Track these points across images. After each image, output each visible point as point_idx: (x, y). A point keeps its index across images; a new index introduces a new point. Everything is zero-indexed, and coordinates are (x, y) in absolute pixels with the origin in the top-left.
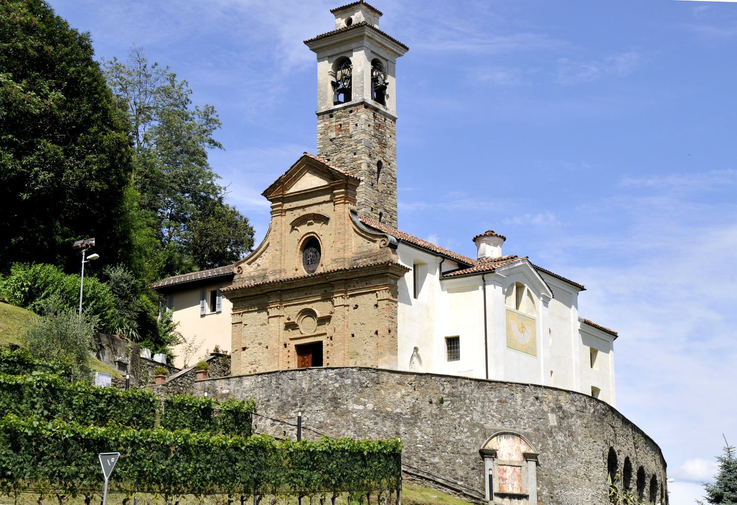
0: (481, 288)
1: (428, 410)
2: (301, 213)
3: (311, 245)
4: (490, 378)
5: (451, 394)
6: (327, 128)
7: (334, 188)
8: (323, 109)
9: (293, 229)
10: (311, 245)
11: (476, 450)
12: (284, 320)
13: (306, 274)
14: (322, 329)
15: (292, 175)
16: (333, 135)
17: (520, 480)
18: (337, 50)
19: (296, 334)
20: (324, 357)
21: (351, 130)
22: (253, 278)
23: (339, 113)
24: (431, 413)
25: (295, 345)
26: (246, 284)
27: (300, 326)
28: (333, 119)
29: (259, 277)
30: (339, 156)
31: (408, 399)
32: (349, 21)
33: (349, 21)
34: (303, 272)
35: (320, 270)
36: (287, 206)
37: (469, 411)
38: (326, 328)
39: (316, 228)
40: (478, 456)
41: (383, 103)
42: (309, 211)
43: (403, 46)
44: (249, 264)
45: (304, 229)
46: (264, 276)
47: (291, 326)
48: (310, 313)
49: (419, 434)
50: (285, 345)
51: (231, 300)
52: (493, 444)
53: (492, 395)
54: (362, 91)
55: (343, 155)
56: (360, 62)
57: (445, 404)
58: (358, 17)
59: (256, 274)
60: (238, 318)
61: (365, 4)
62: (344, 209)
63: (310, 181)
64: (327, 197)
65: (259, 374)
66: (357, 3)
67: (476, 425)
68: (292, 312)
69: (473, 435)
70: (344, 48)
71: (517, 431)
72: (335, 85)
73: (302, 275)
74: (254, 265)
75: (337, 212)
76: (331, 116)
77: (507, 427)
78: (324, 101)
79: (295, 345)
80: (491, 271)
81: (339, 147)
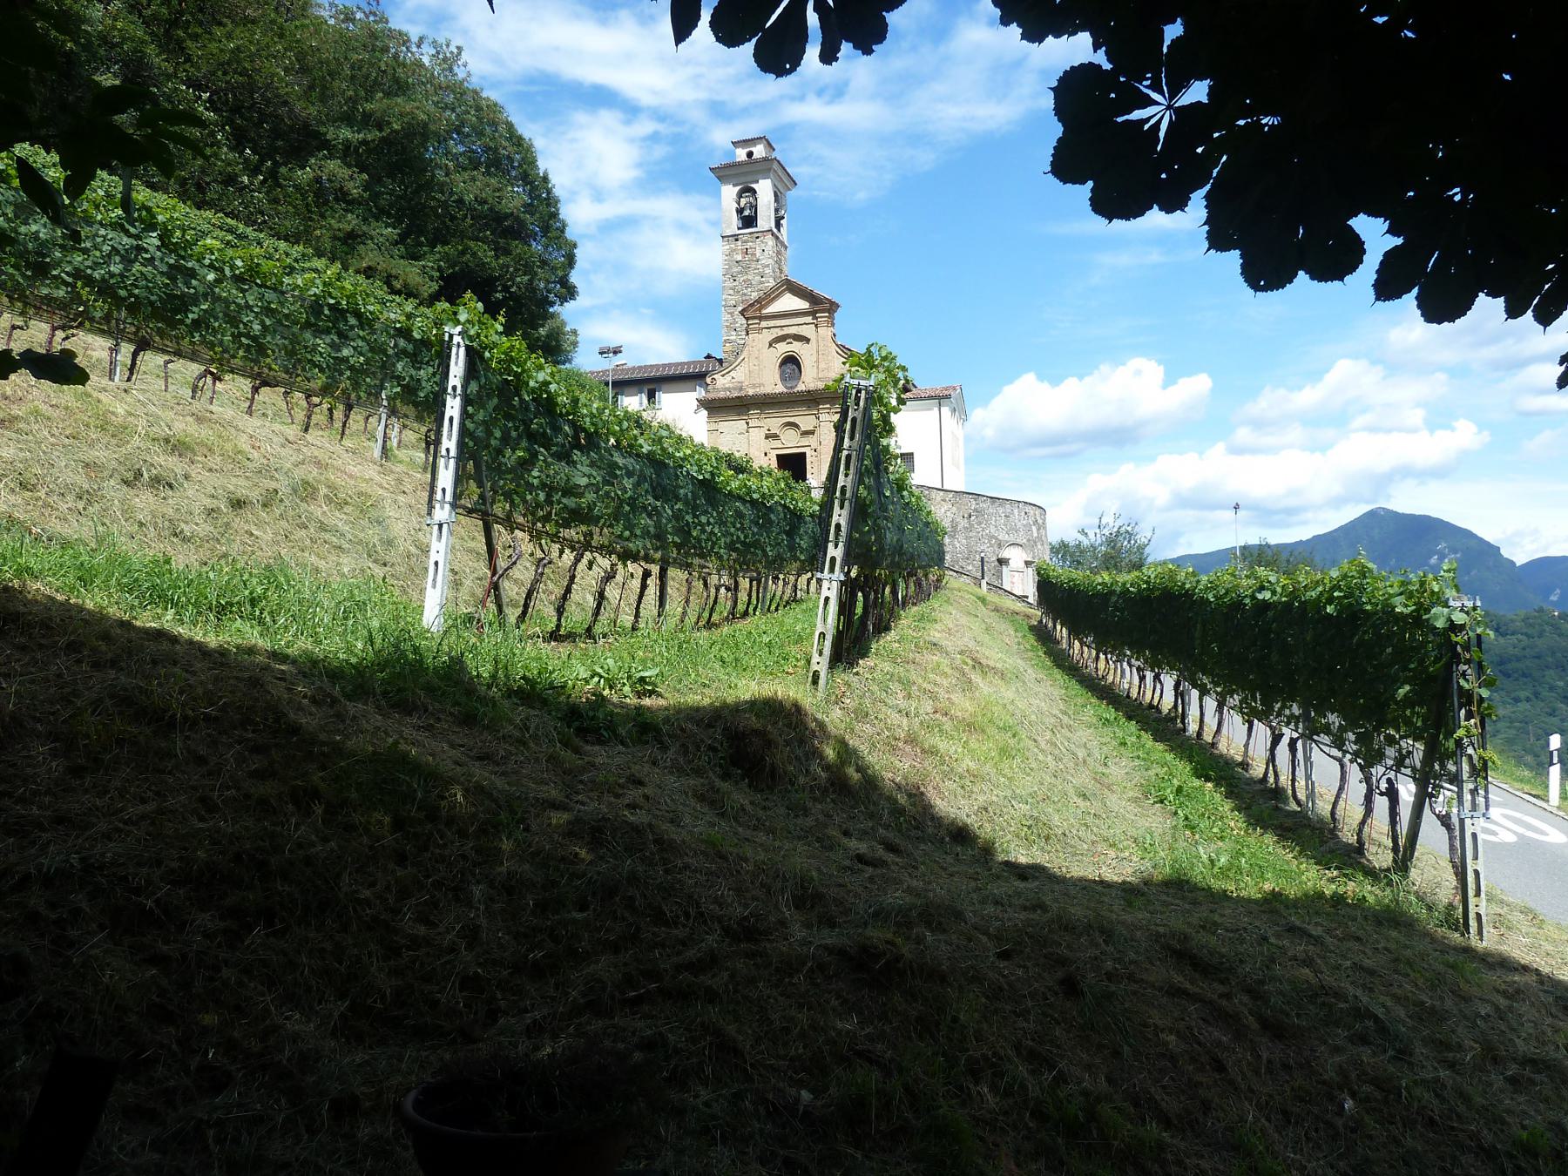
0: (936, 409)
1: (963, 523)
2: (780, 333)
3: (791, 363)
4: (945, 488)
5: (975, 510)
6: (733, 251)
7: (817, 312)
8: (729, 233)
9: (770, 345)
10: (791, 363)
11: (994, 558)
12: (764, 432)
13: (785, 390)
14: (805, 441)
15: (770, 297)
16: (739, 258)
17: (1023, 584)
18: (743, 179)
19: (777, 444)
20: (808, 467)
21: (758, 255)
22: (729, 389)
23: (745, 238)
24: (964, 527)
25: (778, 456)
26: (722, 395)
27: (782, 437)
28: (739, 243)
29: (735, 389)
30: (745, 277)
31: (948, 514)
32: (750, 154)
33: (750, 154)
34: (780, 389)
35: (801, 387)
36: (764, 324)
37: (988, 525)
38: (812, 441)
39: (796, 347)
40: (996, 563)
41: (779, 231)
42: (786, 331)
43: (794, 182)
44: (723, 376)
45: (783, 348)
46: (741, 389)
47: (771, 436)
48: (795, 425)
49: (958, 545)
50: (766, 454)
51: (706, 409)
52: (1005, 554)
53: (1001, 510)
54: (765, 220)
55: (750, 277)
56: (764, 188)
57: (973, 518)
58: (759, 151)
59: (731, 385)
60: (714, 426)
61: (767, 140)
62: (825, 332)
63: (789, 302)
64: (809, 319)
65: (343, 431)
66: (761, 138)
67: (993, 537)
68: (774, 422)
69: (991, 546)
70: (749, 178)
71: (1018, 541)
72: (740, 211)
73: (781, 391)
74: (728, 378)
75: (820, 335)
76: (737, 240)
77: (1012, 539)
78: (729, 226)
79: (778, 456)
80: (948, 397)
81: (745, 270)
